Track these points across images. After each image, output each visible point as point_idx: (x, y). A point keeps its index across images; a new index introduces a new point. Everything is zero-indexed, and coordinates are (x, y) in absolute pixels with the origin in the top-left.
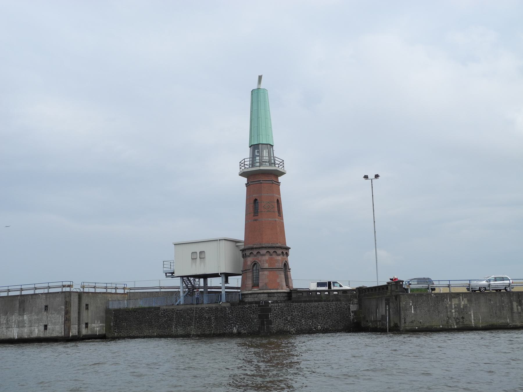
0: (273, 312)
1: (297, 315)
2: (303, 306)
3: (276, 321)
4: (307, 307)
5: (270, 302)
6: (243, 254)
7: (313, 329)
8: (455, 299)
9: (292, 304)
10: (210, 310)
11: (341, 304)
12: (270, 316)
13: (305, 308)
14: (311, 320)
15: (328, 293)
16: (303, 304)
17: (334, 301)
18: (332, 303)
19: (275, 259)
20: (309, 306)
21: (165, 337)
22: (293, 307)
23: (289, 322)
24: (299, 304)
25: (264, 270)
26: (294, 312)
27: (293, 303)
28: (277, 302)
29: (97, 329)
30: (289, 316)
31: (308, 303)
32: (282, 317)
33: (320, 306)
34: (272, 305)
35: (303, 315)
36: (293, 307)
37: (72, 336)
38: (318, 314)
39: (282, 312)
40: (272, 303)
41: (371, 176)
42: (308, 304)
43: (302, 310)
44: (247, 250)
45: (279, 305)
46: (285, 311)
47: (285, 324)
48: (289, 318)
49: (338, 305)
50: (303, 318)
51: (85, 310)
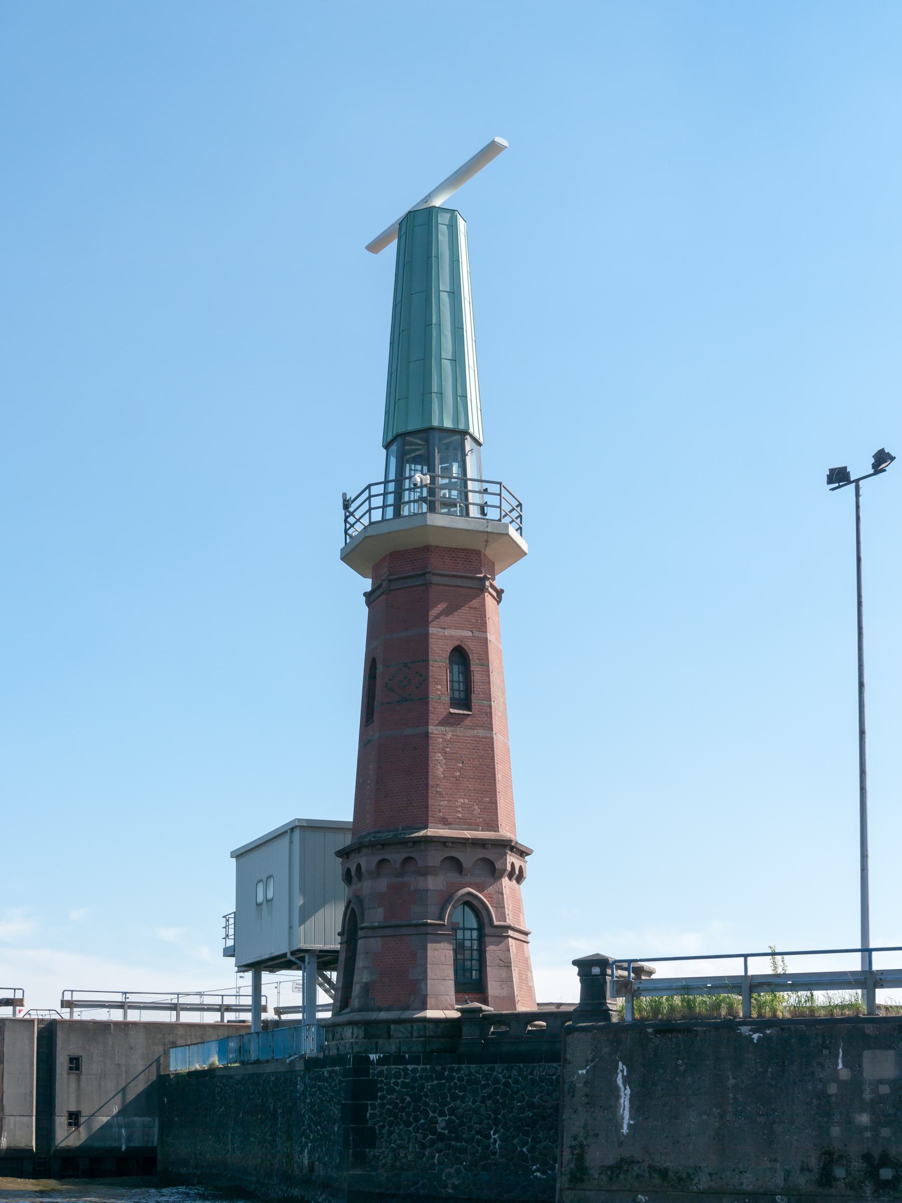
0: (382, 1097)
3: (390, 1133)
4: (516, 1082)
5: (373, 1057)
6: (348, 871)
8: (878, 1052)
9: (456, 1066)
10: (431, 1076)
12: (370, 1111)
13: (506, 1084)
14: (527, 1134)
15: (546, 1024)
19: (412, 888)
22: (460, 1079)
23: (441, 1137)
24: (486, 1067)
25: (405, 931)
26: (463, 1101)
27: (460, 1062)
28: (399, 1059)
30: (442, 1114)
31: (521, 1065)
32: (417, 1119)
34: (382, 1071)
35: (496, 1112)
40: (380, 1062)
41: (860, 466)
44: (364, 851)
45: (405, 1070)
47: (423, 1146)
48: (441, 1122)
50: (497, 1125)
51: (65, 1075)
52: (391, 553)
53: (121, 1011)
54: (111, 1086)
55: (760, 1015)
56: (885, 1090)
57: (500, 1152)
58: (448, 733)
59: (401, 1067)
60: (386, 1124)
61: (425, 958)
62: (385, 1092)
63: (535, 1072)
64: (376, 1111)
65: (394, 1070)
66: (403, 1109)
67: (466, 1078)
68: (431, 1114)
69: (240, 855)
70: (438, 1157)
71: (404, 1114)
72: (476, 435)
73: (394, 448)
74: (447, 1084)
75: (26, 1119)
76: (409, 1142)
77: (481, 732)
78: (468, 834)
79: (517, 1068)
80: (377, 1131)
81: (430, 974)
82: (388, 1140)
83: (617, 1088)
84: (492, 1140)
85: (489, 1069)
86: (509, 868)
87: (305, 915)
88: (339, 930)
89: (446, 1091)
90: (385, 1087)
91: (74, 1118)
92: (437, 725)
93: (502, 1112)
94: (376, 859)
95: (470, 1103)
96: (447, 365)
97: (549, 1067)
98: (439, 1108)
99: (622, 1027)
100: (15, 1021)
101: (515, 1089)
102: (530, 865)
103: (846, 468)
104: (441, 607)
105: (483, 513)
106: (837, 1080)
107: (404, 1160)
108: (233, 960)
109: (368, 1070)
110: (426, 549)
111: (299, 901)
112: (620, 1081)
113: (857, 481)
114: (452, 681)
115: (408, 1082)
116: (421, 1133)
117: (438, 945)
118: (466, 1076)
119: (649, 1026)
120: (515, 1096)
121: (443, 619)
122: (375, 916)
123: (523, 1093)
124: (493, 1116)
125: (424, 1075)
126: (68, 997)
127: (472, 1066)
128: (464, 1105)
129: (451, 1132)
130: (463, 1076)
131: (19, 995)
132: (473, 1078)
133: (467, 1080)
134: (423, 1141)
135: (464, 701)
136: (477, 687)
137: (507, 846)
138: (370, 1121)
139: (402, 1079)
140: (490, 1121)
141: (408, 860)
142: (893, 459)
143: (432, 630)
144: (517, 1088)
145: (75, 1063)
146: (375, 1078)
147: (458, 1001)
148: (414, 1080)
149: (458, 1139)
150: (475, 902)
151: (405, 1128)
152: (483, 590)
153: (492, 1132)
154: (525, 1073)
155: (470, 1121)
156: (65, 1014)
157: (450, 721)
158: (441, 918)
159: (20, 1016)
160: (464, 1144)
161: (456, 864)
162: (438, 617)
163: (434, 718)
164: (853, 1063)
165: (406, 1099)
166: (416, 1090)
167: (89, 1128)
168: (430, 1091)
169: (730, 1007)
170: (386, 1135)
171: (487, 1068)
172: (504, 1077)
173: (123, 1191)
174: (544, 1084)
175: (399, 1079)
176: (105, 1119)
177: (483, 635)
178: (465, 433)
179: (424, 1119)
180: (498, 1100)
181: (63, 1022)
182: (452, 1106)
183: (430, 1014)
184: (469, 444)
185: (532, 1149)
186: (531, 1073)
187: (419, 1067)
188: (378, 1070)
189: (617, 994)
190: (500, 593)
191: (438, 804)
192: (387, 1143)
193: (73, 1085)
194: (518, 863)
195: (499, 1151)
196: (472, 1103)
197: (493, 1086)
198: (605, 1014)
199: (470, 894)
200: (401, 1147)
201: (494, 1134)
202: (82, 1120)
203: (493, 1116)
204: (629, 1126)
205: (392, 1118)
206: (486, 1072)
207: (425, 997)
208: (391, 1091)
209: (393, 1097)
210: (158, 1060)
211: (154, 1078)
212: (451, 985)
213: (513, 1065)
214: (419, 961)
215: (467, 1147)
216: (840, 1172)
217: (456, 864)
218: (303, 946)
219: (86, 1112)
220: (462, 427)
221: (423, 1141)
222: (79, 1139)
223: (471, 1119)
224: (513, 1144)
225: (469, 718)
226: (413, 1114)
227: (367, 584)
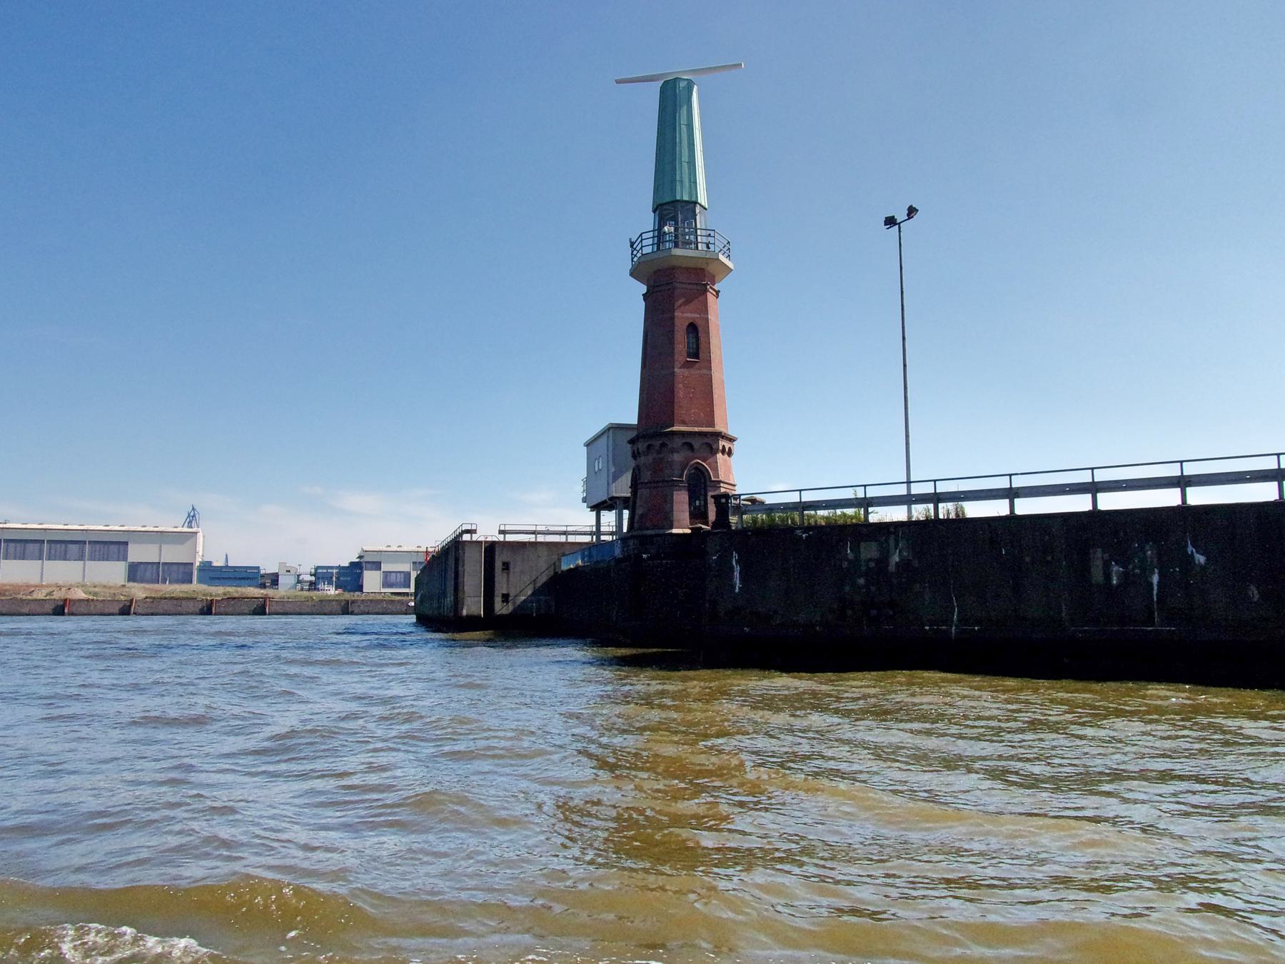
41: (901, 216)
52: (655, 272)
53: (534, 536)
54: (527, 579)
55: (809, 524)
56: (872, 564)
58: (686, 372)
61: (672, 500)
69: (588, 445)
72: (703, 204)
73: (657, 213)
75: (477, 599)
77: (705, 371)
78: (696, 429)
81: (675, 508)
83: (733, 567)
86: (721, 448)
87: (616, 477)
88: (629, 485)
91: (506, 598)
92: (681, 368)
94: (646, 445)
96: (685, 165)
99: (737, 532)
100: (471, 542)
102: (736, 447)
103: (894, 217)
104: (680, 302)
105: (708, 247)
106: (847, 560)
108: (585, 504)
110: (673, 268)
111: (613, 470)
112: (734, 563)
113: (899, 224)
114: (688, 343)
117: (679, 492)
119: (750, 531)
121: (683, 307)
122: (646, 476)
126: (502, 528)
131: (474, 528)
135: (696, 354)
136: (702, 346)
137: (719, 435)
141: (663, 445)
142: (917, 211)
143: (676, 314)
145: (506, 566)
147: (691, 524)
150: (701, 467)
152: (706, 291)
156: (501, 538)
157: (687, 365)
158: (681, 476)
159: (474, 539)
161: (690, 447)
162: (680, 306)
163: (677, 364)
164: (856, 549)
167: (514, 604)
169: (793, 519)
173: (551, 641)
176: (523, 598)
177: (705, 316)
178: (696, 203)
181: (499, 542)
183: (675, 531)
184: (698, 209)
189: (734, 514)
190: (718, 292)
191: (679, 412)
193: (505, 580)
194: (727, 445)
198: (728, 525)
199: (698, 463)
202: (510, 598)
204: (739, 588)
207: (672, 522)
210: (554, 564)
211: (552, 573)
212: (687, 515)
214: (668, 500)
216: (849, 612)
217: (690, 447)
218: (615, 495)
219: (512, 594)
220: (693, 199)
222: (508, 610)
225: (698, 364)
227: (644, 289)
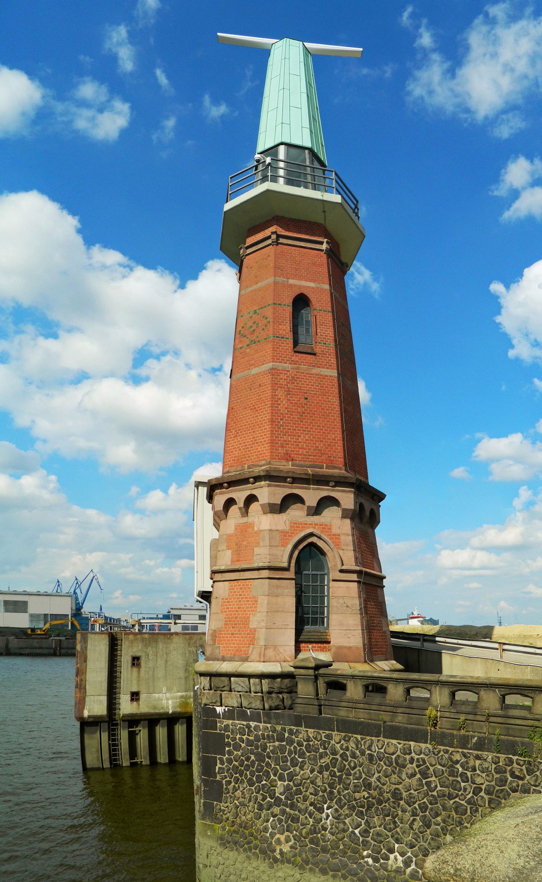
1: (312, 782)
2: (338, 746)
3: (235, 789)
4: (354, 756)
7: (363, 858)
9: (294, 728)
11: (530, 772)
12: (219, 765)
14: (360, 814)
16: (336, 736)
17: (489, 750)
18: (478, 757)
20: (363, 753)
21: (510, 707)
23: (278, 803)
24: (323, 734)
26: (302, 768)
29: (167, 703)
30: (281, 778)
31: (359, 737)
32: (259, 780)
33: (412, 761)
34: (228, 725)
35: (332, 786)
36: (300, 744)
37: (89, 717)
38: (396, 795)
39: (260, 758)
42: (357, 743)
43: (334, 762)
45: (249, 727)
46: (269, 757)
47: (261, 807)
48: (280, 787)
49: (513, 774)
50: (331, 800)
57: (331, 828)
59: (245, 723)
60: (232, 780)
62: (232, 748)
63: (373, 747)
64: (224, 766)
65: (239, 726)
66: (247, 767)
67: (305, 743)
68: (272, 777)
70: (272, 821)
71: (248, 773)
74: (288, 747)
76: (250, 801)
79: (354, 740)
80: (225, 787)
82: (233, 795)
84: (324, 815)
85: (327, 736)
89: (286, 754)
90: (232, 743)
91: (135, 696)
93: (338, 787)
95: (308, 771)
97: (388, 744)
98: (280, 771)
101: (352, 764)
107: (243, 818)
109: (216, 722)
115: (252, 740)
116: (262, 794)
118: (305, 741)
120: (352, 772)
123: (361, 769)
124: (328, 789)
125: (266, 734)
127: (310, 730)
128: (302, 772)
129: (286, 798)
130: (302, 739)
132: (311, 743)
133: (306, 745)
134: (262, 802)
138: (218, 775)
139: (246, 736)
140: (325, 794)
144: (355, 762)
146: (223, 732)
148: (257, 739)
149: (292, 806)
151: (248, 787)
153: (325, 806)
154: (363, 747)
155: (307, 791)
160: (297, 812)
165: (251, 757)
166: (260, 750)
168: (273, 752)
170: (231, 791)
171: (325, 734)
172: (342, 749)
174: (382, 763)
175: (244, 735)
179: (266, 780)
180: (335, 773)
182: (292, 772)
185: (365, 833)
186: (369, 748)
187: (261, 725)
188: (225, 724)
192: (232, 799)
195: (329, 827)
196: (310, 771)
197: (331, 757)
200: (243, 804)
201: (328, 809)
203: (328, 789)
205: (238, 775)
206: (324, 739)
208: (237, 747)
209: (239, 753)
213: (350, 735)
215: (299, 816)
221: (262, 802)
223: (307, 788)
224: (344, 823)
226: (257, 774)
